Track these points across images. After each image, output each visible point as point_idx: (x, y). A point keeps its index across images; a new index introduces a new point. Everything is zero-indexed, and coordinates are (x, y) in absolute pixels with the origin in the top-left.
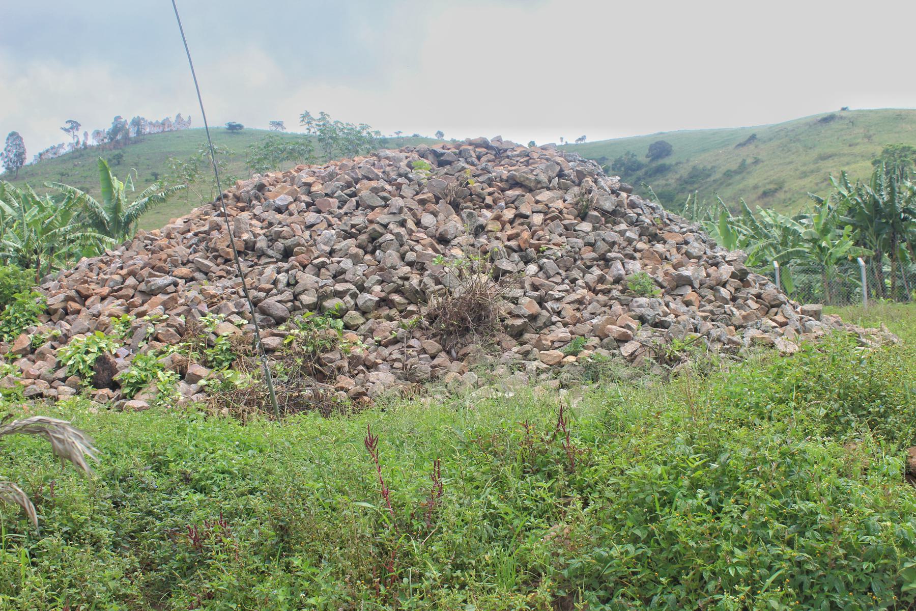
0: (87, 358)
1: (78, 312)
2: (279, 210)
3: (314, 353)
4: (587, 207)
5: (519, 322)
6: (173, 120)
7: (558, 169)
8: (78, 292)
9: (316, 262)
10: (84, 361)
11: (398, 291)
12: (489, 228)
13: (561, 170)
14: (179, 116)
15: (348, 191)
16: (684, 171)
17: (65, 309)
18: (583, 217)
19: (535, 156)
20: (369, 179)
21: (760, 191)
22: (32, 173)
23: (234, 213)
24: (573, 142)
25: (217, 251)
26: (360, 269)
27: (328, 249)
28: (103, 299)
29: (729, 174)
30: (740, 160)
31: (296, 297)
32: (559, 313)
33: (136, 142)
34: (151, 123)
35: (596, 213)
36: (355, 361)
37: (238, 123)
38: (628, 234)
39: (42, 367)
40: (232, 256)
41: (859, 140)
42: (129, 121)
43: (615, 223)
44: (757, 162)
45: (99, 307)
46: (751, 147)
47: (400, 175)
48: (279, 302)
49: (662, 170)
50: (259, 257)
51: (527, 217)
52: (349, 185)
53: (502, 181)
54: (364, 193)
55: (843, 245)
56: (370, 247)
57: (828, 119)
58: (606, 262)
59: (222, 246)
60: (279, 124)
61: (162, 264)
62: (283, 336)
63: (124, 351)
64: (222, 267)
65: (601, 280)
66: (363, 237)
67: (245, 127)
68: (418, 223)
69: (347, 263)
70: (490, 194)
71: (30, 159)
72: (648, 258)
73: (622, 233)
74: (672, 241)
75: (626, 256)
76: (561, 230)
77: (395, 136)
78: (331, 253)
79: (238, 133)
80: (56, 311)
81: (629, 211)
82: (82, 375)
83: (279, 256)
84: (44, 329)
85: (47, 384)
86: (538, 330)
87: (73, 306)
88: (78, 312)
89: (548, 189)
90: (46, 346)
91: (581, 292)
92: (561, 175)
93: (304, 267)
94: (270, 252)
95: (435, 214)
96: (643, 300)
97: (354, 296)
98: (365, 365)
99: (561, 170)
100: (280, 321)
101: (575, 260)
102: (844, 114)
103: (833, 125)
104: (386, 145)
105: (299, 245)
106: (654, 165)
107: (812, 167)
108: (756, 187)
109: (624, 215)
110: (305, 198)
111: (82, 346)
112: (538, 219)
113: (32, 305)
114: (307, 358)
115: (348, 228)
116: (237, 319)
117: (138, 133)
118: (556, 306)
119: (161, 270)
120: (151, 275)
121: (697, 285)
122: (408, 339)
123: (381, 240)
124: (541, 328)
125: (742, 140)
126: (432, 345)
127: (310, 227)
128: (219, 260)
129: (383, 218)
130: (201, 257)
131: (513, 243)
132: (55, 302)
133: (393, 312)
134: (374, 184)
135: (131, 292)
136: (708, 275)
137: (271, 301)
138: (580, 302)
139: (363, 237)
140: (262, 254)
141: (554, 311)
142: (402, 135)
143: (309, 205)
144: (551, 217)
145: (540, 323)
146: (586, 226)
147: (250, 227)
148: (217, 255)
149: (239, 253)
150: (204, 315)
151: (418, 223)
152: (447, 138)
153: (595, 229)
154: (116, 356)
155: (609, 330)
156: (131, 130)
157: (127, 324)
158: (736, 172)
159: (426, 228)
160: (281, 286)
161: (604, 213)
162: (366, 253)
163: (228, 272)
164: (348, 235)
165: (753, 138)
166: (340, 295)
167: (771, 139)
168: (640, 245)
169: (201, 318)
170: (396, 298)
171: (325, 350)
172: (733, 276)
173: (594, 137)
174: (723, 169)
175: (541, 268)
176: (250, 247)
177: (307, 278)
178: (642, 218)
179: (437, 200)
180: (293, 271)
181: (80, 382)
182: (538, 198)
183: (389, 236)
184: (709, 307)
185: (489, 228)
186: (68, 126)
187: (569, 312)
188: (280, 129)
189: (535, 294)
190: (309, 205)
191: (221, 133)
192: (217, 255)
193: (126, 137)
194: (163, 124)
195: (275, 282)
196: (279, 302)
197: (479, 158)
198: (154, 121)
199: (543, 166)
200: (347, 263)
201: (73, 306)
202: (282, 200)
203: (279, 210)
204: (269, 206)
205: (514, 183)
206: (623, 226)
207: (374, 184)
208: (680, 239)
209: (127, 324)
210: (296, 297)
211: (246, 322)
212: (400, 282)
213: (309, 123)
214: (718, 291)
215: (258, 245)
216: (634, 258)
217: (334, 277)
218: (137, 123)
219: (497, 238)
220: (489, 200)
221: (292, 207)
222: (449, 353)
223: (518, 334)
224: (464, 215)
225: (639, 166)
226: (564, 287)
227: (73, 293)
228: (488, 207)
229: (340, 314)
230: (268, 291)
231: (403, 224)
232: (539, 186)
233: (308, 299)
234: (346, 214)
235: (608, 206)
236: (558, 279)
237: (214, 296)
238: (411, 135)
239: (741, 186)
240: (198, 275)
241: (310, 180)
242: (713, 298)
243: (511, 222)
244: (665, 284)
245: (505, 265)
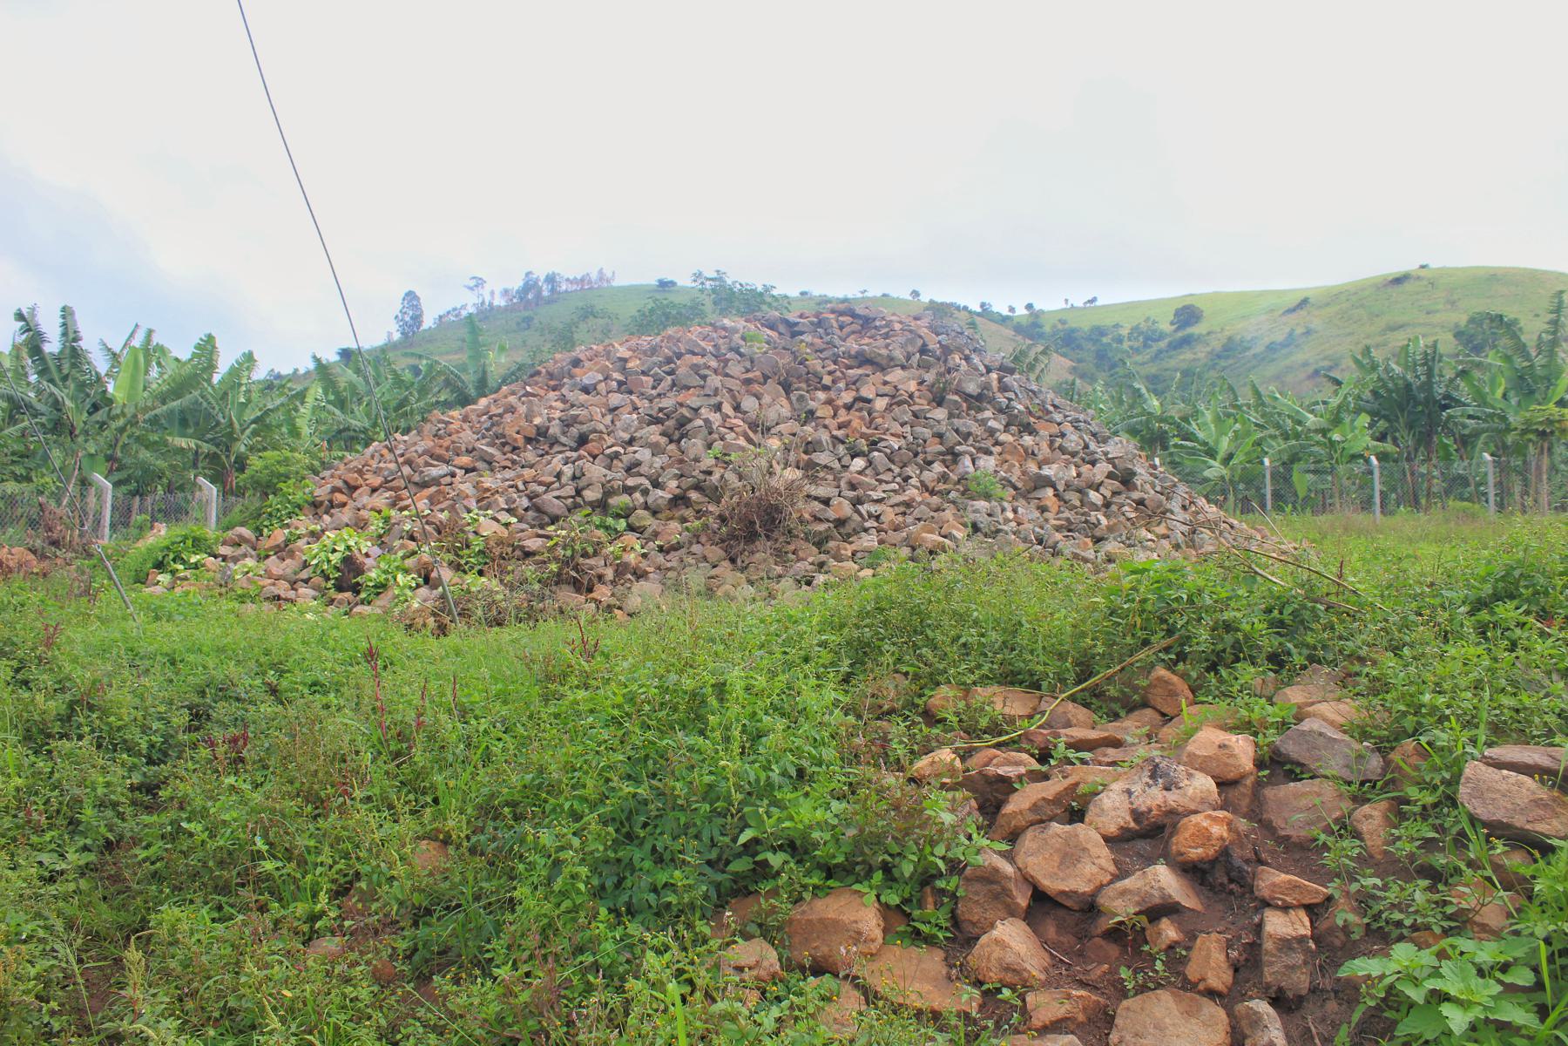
0: (332, 557)
1: (344, 505)
2: (586, 390)
3: (573, 557)
4: (944, 390)
5: (821, 527)
6: (594, 276)
7: (920, 342)
8: (346, 482)
9: (608, 451)
10: (329, 561)
11: (697, 487)
12: (819, 414)
13: (924, 345)
14: (601, 272)
15: (666, 368)
16: (1216, 344)
17: (331, 501)
18: (939, 401)
19: (897, 326)
20: (694, 354)
21: (1310, 370)
22: (430, 337)
23: (542, 393)
24: (1080, 304)
25: (504, 436)
26: (658, 461)
27: (626, 437)
28: (374, 490)
29: (1271, 348)
30: (1287, 330)
31: (578, 492)
32: (877, 518)
33: (549, 302)
35: (956, 398)
36: (621, 570)
38: (991, 423)
39: (289, 566)
40: (521, 443)
41: (1440, 307)
42: (542, 278)
43: (980, 410)
44: (1308, 332)
45: (365, 499)
46: (1303, 313)
47: (731, 349)
48: (557, 498)
49: (1186, 341)
50: (551, 446)
51: (869, 401)
52: (669, 361)
53: (850, 357)
54: (682, 371)
55: (1359, 434)
56: (677, 435)
57: (1398, 281)
58: (953, 456)
59: (511, 432)
61: (443, 452)
62: (549, 537)
63: (376, 551)
64: (509, 455)
65: (944, 478)
66: (670, 423)
68: (737, 408)
69: (644, 454)
70: (830, 373)
71: (428, 322)
72: (1011, 453)
73: (983, 422)
74: (1044, 433)
75: (979, 450)
76: (908, 417)
78: (631, 442)
80: (322, 503)
81: (998, 395)
82: (327, 579)
83: (574, 445)
84: (304, 523)
85: (287, 585)
86: (846, 538)
87: (340, 497)
88: (344, 505)
89: (903, 368)
90: (300, 543)
91: (912, 492)
92: (924, 350)
93: (595, 457)
94: (563, 439)
95: (758, 397)
96: (982, 504)
97: (645, 492)
98: (634, 573)
99: (924, 345)
100: (554, 520)
101: (916, 455)
102: (1422, 273)
103: (1408, 287)
105: (595, 431)
106: (1180, 334)
107: (1379, 339)
108: (1305, 364)
109: (992, 401)
110: (616, 375)
111: (338, 540)
112: (881, 404)
113: (299, 497)
114: (565, 563)
115: (653, 413)
116: (505, 517)
117: (553, 290)
118: (873, 508)
119: (440, 458)
120: (427, 464)
121: (1061, 488)
122: (691, 543)
123: (688, 427)
124: (849, 535)
125: (1292, 306)
126: (715, 552)
127: (613, 410)
128: (507, 448)
129: (694, 401)
130: (488, 445)
131: (839, 433)
132: (322, 493)
133: (689, 513)
134: (697, 360)
135: (402, 483)
136: (1079, 475)
137: (549, 497)
138: (908, 504)
139: (670, 423)
140: (555, 442)
141: (870, 515)
142: (869, 294)
143: (620, 384)
144: (896, 400)
145: (848, 529)
146: (940, 414)
147: (549, 411)
148: (504, 443)
149: (529, 440)
150: (469, 511)
151: (737, 408)
152: (925, 298)
153: (951, 416)
154: (367, 555)
155: (924, 540)
157: (387, 520)
158: (1284, 345)
159: (745, 413)
160: (564, 480)
161: (967, 397)
162: (671, 441)
163: (514, 462)
164: (655, 421)
165: (1304, 302)
166: (629, 490)
167: (1327, 305)
168: (1003, 437)
169: (465, 515)
170: (694, 495)
171: (585, 555)
172: (1110, 476)
173: (1109, 296)
174: (1267, 341)
175: (870, 463)
176: (542, 432)
177: (596, 471)
178: (1014, 403)
179: (766, 378)
180: (580, 463)
181: (323, 584)
182: (887, 378)
183: (699, 422)
184: (1067, 514)
185: (819, 414)
186: (472, 283)
187: (889, 515)
189: (852, 494)
190: (620, 384)
192: (504, 443)
193: (539, 295)
194: (582, 280)
195: (559, 476)
196: (557, 498)
197: (841, 328)
199: (901, 339)
200: (644, 454)
201: (340, 497)
202: (588, 378)
203: (586, 390)
204: (575, 385)
205: (863, 360)
206: (988, 414)
207: (697, 360)
208: (1055, 429)
209: (387, 520)
210: (578, 492)
211: (514, 520)
212: (702, 477)
214: (1087, 494)
215: (551, 431)
216: (991, 453)
217: (628, 470)
218: (551, 279)
219: (825, 427)
220: (827, 380)
221: (602, 387)
222: (733, 561)
223: (820, 543)
224: (794, 399)
225: (1161, 337)
226: (895, 486)
227: (339, 484)
228: (826, 388)
229: (627, 513)
230: (548, 485)
231: (718, 408)
233: (591, 495)
234: (659, 395)
235: (972, 388)
236: (887, 477)
237: (488, 490)
238: (879, 294)
239: (1288, 362)
240: (480, 465)
241: (627, 354)
242: (1078, 503)
243: (848, 407)
244: (1020, 485)
245: (822, 458)
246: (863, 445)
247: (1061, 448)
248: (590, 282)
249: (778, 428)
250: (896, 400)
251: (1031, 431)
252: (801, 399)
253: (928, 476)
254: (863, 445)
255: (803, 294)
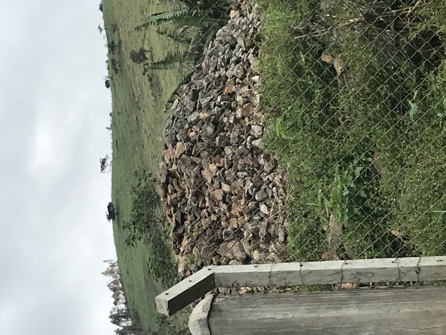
6: (110, 279)
14: (106, 273)
18: (220, 152)
33: (136, 318)
34: (115, 303)
35: (217, 139)
37: (107, 210)
42: (116, 327)
58: (254, 151)
60: (103, 162)
65: (267, 158)
67: (111, 201)
77: (104, 32)
79: (118, 208)
89: (202, 169)
92: (189, 153)
104: (116, 43)
109: (218, 116)
117: (126, 316)
146: (228, 151)
153: (228, 144)
156: (124, 324)
168: (239, 113)
188: (109, 162)
191: (118, 223)
194: (114, 290)
198: (113, 300)
213: (134, 239)
232: (199, 176)
238: (101, 14)
246: (251, 204)
247: (241, 79)
248: (115, 282)
249: (247, 251)
250: (223, 178)
251: (232, 95)
252: (227, 234)
253: (267, 169)
254: (251, 204)
255: (107, 85)
